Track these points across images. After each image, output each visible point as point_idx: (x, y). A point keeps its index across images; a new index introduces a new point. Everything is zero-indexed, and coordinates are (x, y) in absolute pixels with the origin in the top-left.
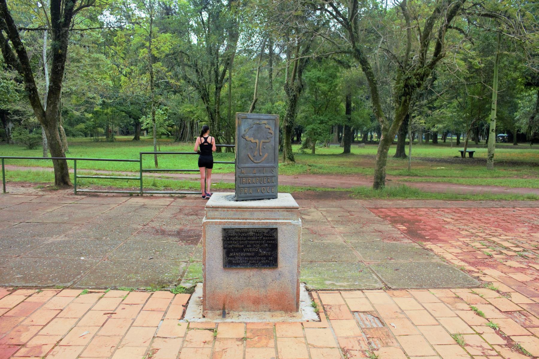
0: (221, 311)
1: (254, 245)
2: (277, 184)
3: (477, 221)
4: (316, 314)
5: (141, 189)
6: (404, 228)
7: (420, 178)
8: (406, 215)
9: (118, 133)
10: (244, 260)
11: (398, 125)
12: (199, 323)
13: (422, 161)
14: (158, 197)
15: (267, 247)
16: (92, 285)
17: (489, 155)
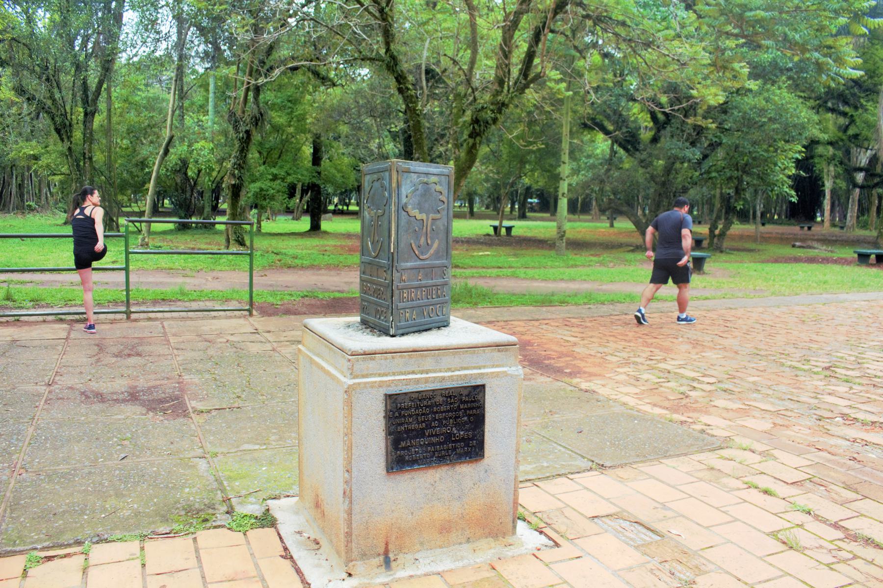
0: (382, 558)
1: (444, 422)
4: (538, 533)
10: (426, 452)
14: (33, 322)
15: (466, 423)
16: (39, 541)
17: (558, 233)
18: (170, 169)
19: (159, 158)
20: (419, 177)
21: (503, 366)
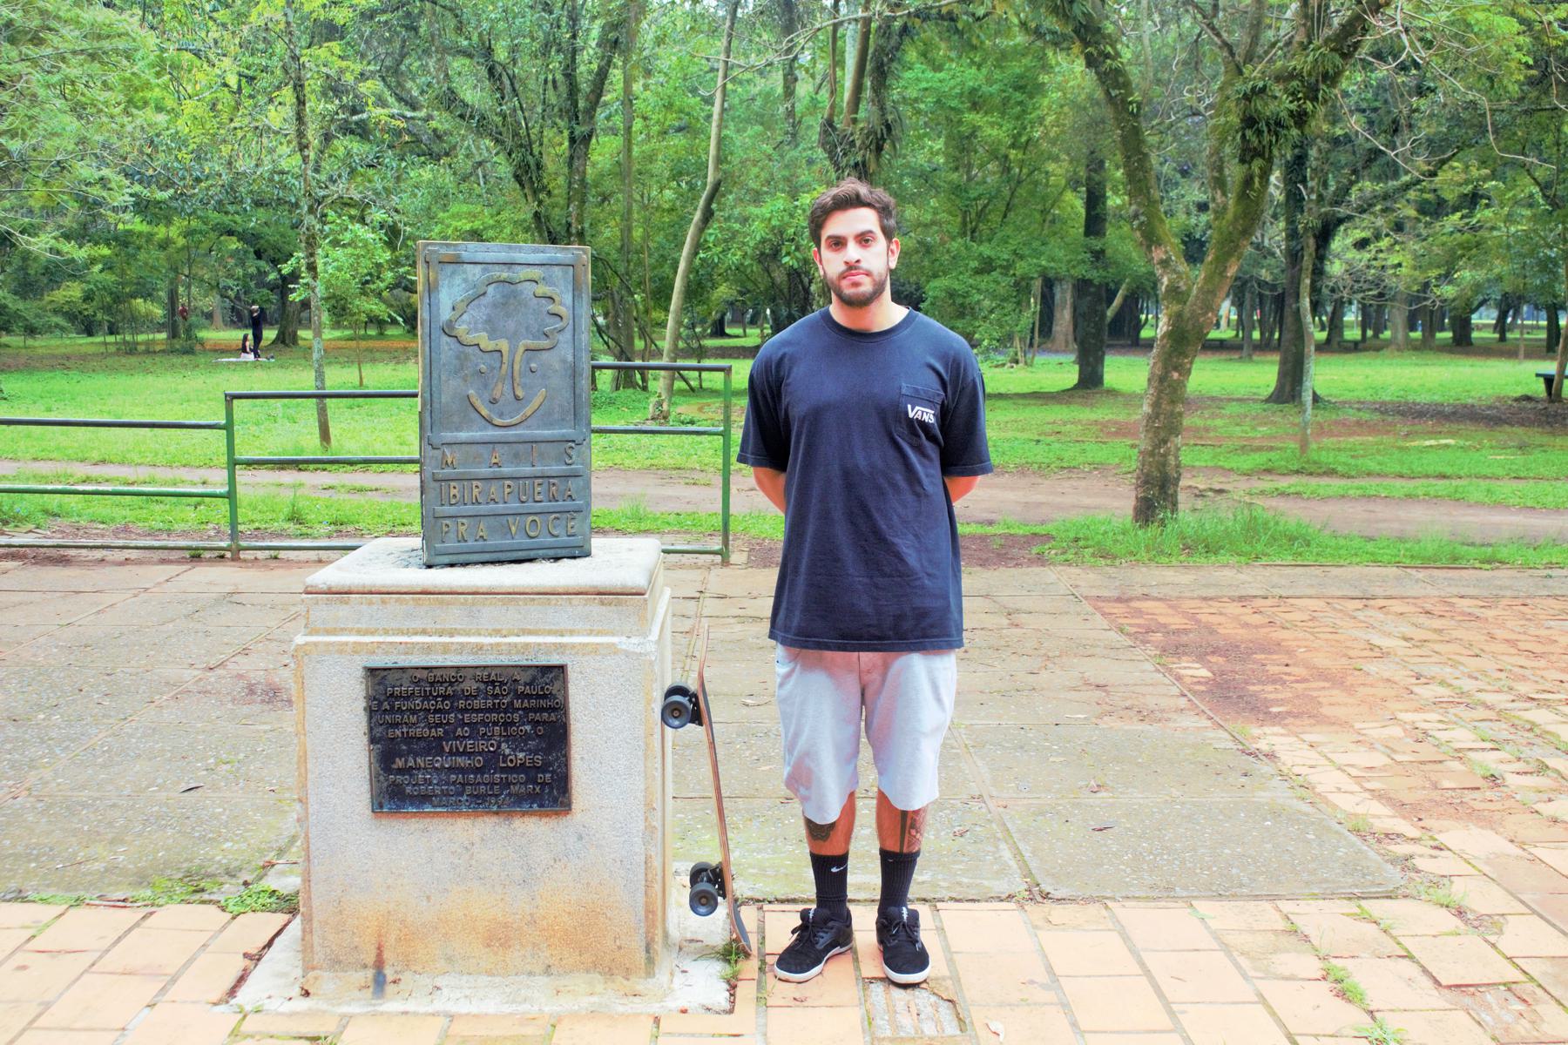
0: (370, 973)
2: (589, 505)
3: (1503, 648)
5: (235, 534)
6: (1204, 673)
7: (1343, 483)
8: (1230, 623)
9: (218, 317)
10: (447, 783)
11: (1222, 274)
12: (282, 1014)
13: (1376, 417)
15: (527, 737)
18: (749, 251)
19: (691, 230)
20: (484, 271)
21: (613, 635)
